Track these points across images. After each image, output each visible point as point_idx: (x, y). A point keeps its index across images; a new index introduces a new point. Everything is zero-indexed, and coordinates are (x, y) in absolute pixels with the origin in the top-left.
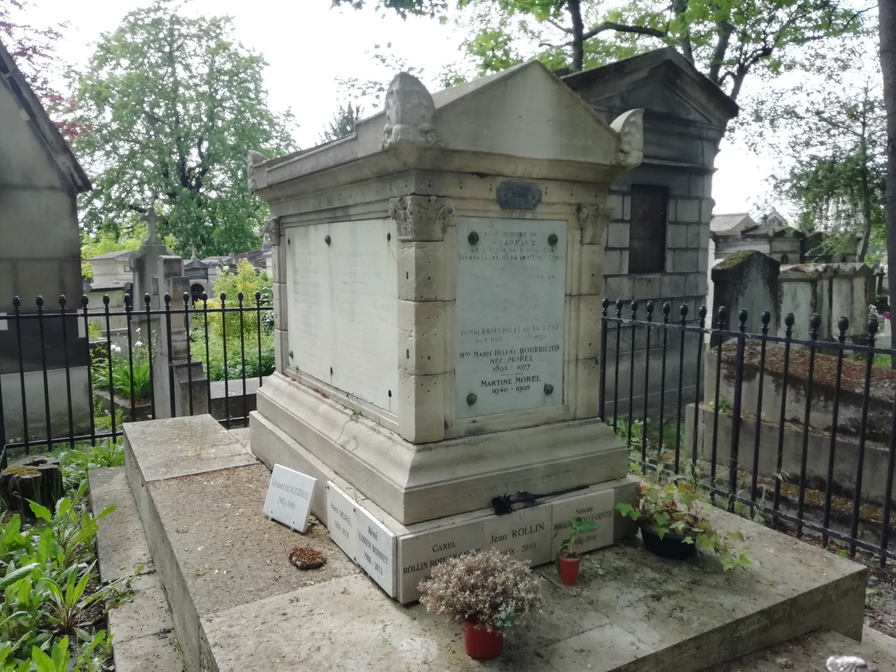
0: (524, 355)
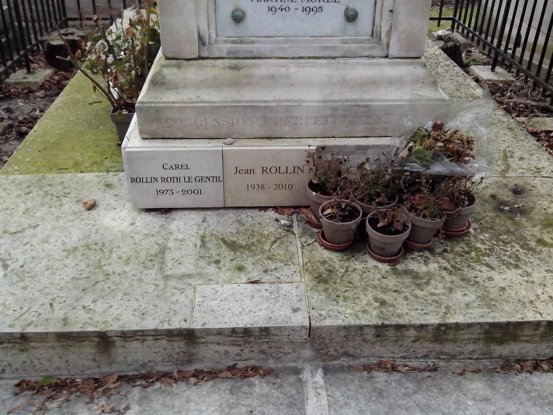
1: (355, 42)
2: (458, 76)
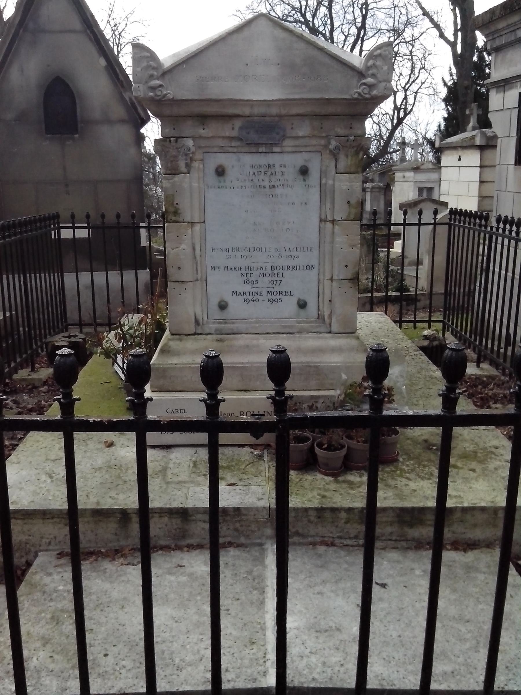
0: (276, 272)
1: (306, 322)
2: (422, 363)
